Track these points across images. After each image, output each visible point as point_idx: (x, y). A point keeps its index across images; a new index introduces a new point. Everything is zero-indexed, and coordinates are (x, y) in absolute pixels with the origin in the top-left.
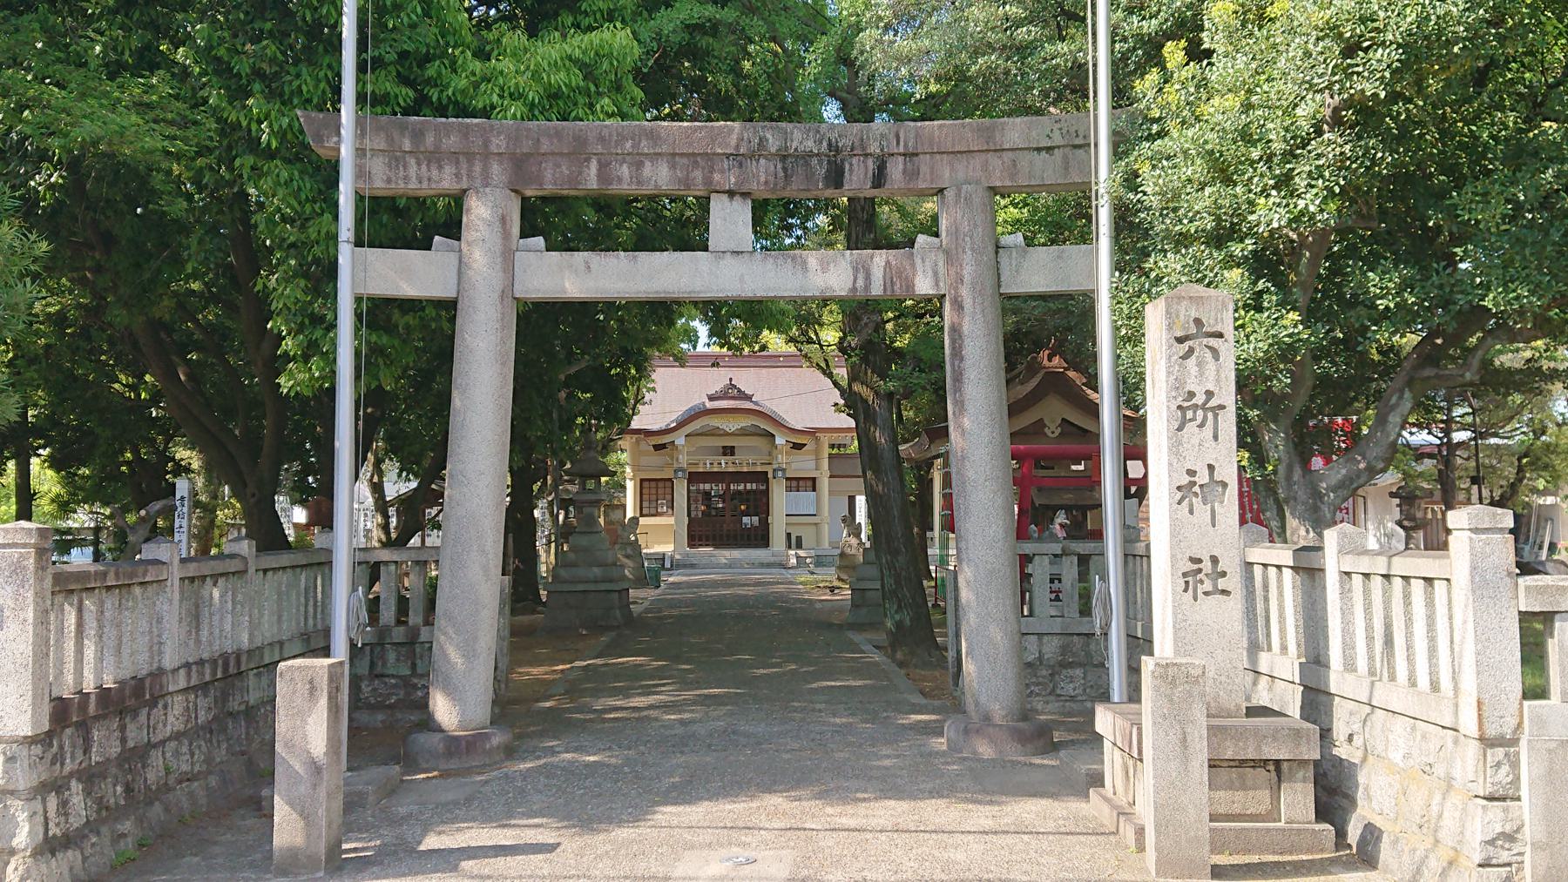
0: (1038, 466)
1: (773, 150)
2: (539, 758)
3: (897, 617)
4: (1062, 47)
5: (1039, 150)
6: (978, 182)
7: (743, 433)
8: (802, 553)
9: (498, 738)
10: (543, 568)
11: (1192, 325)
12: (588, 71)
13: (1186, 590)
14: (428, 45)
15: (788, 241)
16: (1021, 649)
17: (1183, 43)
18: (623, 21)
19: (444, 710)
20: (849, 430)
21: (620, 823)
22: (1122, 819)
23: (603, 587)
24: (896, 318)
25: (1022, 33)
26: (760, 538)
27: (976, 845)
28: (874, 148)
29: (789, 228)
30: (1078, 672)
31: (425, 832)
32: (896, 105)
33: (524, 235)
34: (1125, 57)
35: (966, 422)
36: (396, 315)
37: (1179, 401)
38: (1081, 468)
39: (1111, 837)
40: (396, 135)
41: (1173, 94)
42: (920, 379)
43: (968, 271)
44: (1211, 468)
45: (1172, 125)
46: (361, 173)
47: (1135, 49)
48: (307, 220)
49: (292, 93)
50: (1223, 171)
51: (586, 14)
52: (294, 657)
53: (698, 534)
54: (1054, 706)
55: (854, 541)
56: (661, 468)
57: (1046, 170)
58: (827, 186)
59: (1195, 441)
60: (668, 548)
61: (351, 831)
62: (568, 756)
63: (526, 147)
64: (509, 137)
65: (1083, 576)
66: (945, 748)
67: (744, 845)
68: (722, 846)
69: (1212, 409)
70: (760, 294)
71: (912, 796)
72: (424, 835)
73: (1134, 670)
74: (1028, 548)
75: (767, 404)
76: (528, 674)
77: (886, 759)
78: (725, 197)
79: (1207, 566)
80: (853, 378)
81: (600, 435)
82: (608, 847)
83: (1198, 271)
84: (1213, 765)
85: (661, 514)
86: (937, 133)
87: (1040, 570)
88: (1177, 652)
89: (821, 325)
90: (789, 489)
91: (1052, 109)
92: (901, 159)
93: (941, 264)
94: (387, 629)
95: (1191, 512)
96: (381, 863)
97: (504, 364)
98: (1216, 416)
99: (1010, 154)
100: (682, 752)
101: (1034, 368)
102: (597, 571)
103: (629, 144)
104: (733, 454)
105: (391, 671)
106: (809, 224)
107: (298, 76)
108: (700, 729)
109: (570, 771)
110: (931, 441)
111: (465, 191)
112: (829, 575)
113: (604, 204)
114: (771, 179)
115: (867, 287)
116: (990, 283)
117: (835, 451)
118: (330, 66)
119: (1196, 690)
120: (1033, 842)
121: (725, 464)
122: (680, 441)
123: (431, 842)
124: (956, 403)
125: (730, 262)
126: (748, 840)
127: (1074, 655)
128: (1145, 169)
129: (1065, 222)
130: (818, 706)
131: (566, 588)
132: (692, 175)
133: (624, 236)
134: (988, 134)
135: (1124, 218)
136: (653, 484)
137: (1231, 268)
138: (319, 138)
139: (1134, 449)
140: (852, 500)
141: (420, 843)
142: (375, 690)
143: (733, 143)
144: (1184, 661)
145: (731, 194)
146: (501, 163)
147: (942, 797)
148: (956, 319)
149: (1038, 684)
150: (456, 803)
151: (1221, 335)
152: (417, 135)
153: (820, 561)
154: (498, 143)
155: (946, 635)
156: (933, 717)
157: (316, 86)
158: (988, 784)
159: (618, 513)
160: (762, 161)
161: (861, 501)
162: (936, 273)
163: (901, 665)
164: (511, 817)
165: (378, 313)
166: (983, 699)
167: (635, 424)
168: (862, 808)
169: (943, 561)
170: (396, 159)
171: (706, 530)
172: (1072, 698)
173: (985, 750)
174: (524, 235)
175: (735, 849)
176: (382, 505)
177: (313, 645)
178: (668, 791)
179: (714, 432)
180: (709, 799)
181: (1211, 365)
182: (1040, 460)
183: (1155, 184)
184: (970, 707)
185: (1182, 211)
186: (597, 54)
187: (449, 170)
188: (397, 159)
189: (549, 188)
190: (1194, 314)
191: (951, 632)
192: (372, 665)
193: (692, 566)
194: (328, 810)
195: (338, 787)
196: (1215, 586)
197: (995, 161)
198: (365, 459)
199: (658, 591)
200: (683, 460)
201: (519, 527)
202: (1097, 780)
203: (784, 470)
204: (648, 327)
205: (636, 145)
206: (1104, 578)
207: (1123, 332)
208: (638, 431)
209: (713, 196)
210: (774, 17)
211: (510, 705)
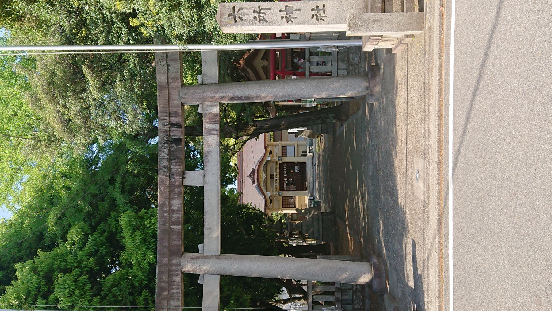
0: (278, 68)
1: (168, 163)
2: (382, 245)
3: (331, 119)
4: (131, 61)
5: (168, 70)
7: (266, 171)
8: (308, 151)
10: (313, 242)
11: (230, 17)
13: (323, 20)
14: (128, 285)
15: (199, 156)
16: (343, 76)
17: (131, 19)
19: (365, 279)
20: (265, 136)
21: (404, 217)
22: (402, 42)
23: (321, 222)
24: (226, 118)
25: (126, 75)
27: (412, 93)
28: (167, 128)
29: (194, 156)
30: (351, 56)
31: (407, 286)
32: (150, 119)
33: (198, 251)
34: (135, 39)
35: (263, 95)
36: (224, 295)
37: (257, 22)
38: (278, 53)
39: (409, 46)
40: (162, 297)
41: (149, 23)
42: (248, 110)
43: (210, 95)
44: (280, 11)
45: (159, 23)
47: (132, 36)
50: (176, 6)
53: (302, 188)
55: (304, 133)
56: (279, 200)
57: (175, 67)
58: (181, 144)
59: (271, 16)
60: (307, 198)
62: (381, 235)
63: (166, 251)
64: (164, 257)
65: (317, 54)
66: (377, 103)
67: (412, 174)
68: (412, 182)
69: (260, 10)
70: (219, 167)
71: (395, 115)
73: (350, 38)
74: (307, 73)
75: (256, 163)
76: (351, 248)
77: (381, 123)
78: (184, 180)
79: (315, 12)
80: (247, 135)
83: (211, 14)
84: (384, 11)
85: (295, 200)
87: (315, 69)
88: (345, 23)
89: (228, 144)
90: (286, 155)
91: (153, 64)
95: (296, 18)
96: (419, 302)
98: (262, 9)
99: (170, 80)
100: (379, 195)
101: (244, 70)
102: (315, 223)
103: (166, 214)
104: (273, 175)
105: (351, 297)
106: (193, 149)
108: (371, 188)
109: (386, 235)
111: (182, 272)
112: (315, 141)
114: (178, 164)
115: (216, 130)
116: (215, 87)
119: (358, 17)
121: (277, 178)
122: (268, 194)
123: (411, 284)
124: (257, 99)
126: (410, 172)
129: (193, 61)
130: (363, 147)
132: (176, 192)
133: (196, 215)
134: (162, 88)
135: (192, 40)
137: (210, 3)
139: (272, 37)
140: (289, 133)
141: (412, 288)
142: (357, 303)
144: (348, 21)
145: (183, 178)
146: (172, 260)
147: (395, 105)
150: (398, 275)
151: (234, 7)
152: (162, 289)
153: (311, 144)
154: (165, 260)
158: (390, 88)
160: (172, 167)
161: (289, 131)
162: (212, 106)
163: (347, 117)
164: (402, 255)
166: (361, 90)
167: (263, 210)
168: (399, 133)
169: (311, 102)
170: (170, 297)
171: (300, 184)
172: (360, 58)
173: (378, 88)
174: (198, 251)
178: (393, 200)
180: (396, 186)
181: (245, 11)
182: (276, 68)
183: (180, 29)
185: (190, 20)
188: (171, 297)
189: (181, 243)
190: (227, 17)
191: (337, 100)
192: (348, 304)
193: (313, 189)
196: (321, 10)
197: (172, 85)
199: (322, 201)
200: (276, 193)
201: (300, 252)
202: (389, 51)
203: (279, 157)
204: (230, 206)
205: (166, 212)
206: (318, 48)
207: (232, 40)
208: (265, 209)
209: (184, 184)
210: (119, 163)
211: (363, 255)
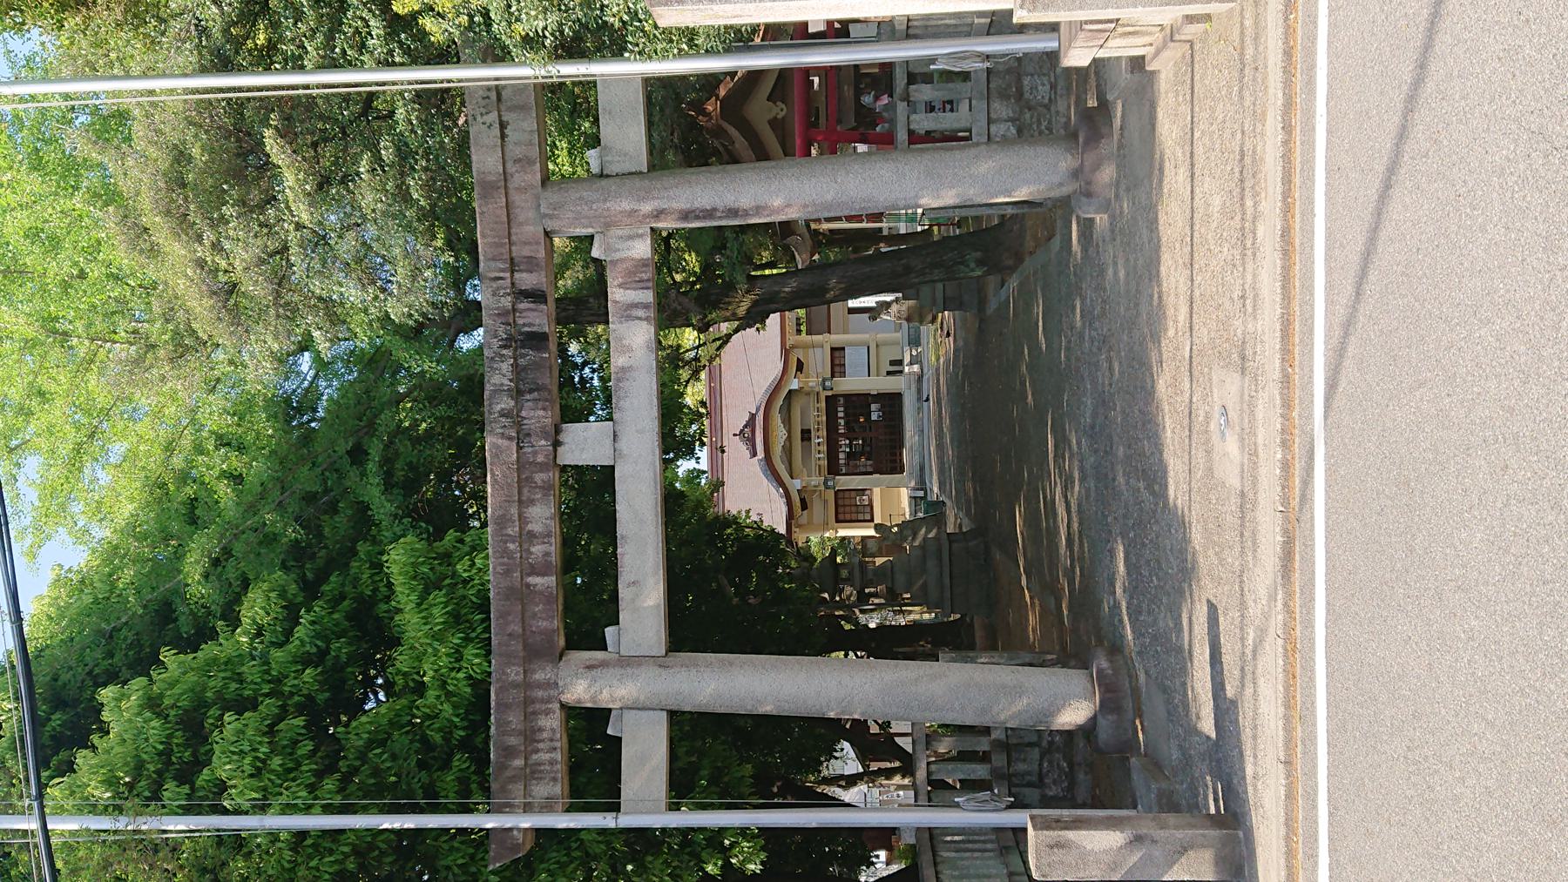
0: (816, 125)
1: (512, 403)
2: (1121, 621)
3: (973, 265)
4: (400, 113)
5: (503, 136)
6: (537, 197)
7: (787, 422)
8: (907, 359)
9: (1101, 662)
10: (926, 616)
12: (429, 586)
14: (412, 741)
16: (1005, 141)
18: (382, 553)
19: (1074, 714)
21: (1186, 540)
22: (1177, 37)
25: (387, 154)
26: (892, 402)
27: (1206, 185)
28: (507, 302)
30: (1026, 81)
32: (457, 279)
33: (603, 646)
34: (407, 51)
36: (680, 764)
38: (816, 80)
39: (1196, 47)
40: (508, 773)
46: (547, 807)
48: (587, 854)
49: (464, 873)
51: (375, 590)
52: (1025, 863)
54: (1061, 105)
55: (895, 307)
57: (523, 128)
58: (546, 349)
60: (904, 494)
61: (1197, 806)
62: (1119, 591)
63: (516, 646)
64: (509, 664)
65: (927, 78)
67: (1208, 417)
72: (1199, 733)
73: (1022, 29)
74: (902, 136)
75: (758, 397)
80: (734, 317)
81: (793, 564)
82: (1211, 552)
85: (871, 501)
86: (490, 240)
87: (923, 123)
89: (679, 346)
90: (843, 374)
91: (461, 122)
92: (517, 275)
93: (620, 233)
94: (993, 771)
96: (1229, 775)
97: (731, 664)
99: (509, 165)
100: (1114, 480)
102: (931, 564)
103: (511, 546)
104: (809, 431)
105: (1036, 767)
106: (579, 360)
107: (448, 868)
109: (1133, 590)
110: (793, 233)
112: (927, 330)
113: (569, 564)
115: (646, 306)
117: (803, 328)
118: (436, 840)
120: (1202, 127)
121: (819, 439)
122: (796, 484)
123: (1207, 726)
125: (622, 441)
126: (1202, 413)
127: (1009, 86)
128: (520, 29)
129: (573, 107)
131: (948, 594)
132: (540, 483)
134: (489, 189)
135: (570, 49)
136: (841, 510)
138: (516, 847)
140: (852, 311)
141: (1208, 738)
142: (1055, 782)
143: (506, 443)
145: (557, 444)
146: (534, 671)
148: (676, 216)
149: (1039, 123)
150: (1168, 702)
152: (509, 752)
153: (915, 341)
155: (989, 217)
156: (1074, 227)
157: (458, 850)
158: (1142, 171)
159: (871, 545)
160: (524, 414)
161: (852, 303)
162: (631, 238)
163: (1019, 259)
165: (681, 789)
166: (1056, 179)
168: (1170, 300)
169: (912, 219)
170: (532, 773)
172: (1053, 87)
174: (603, 646)
175: (1212, 426)
176: (867, 776)
177: (1012, 843)
178: (1153, 493)
179: (788, 450)
182: (810, 124)
183: (536, 18)
184: (1066, 190)
186: (414, 578)
187: (543, 722)
188: (533, 772)
192: (1030, 785)
193: (922, 469)
194: (1177, 828)
195: (1154, 819)
197: (517, 180)
198: (826, 797)
200: (816, 480)
202: (1137, 63)
203: (824, 380)
204: (691, 521)
206: (933, 60)
207: (685, 46)
209: (560, 462)
211: (1070, 655)
